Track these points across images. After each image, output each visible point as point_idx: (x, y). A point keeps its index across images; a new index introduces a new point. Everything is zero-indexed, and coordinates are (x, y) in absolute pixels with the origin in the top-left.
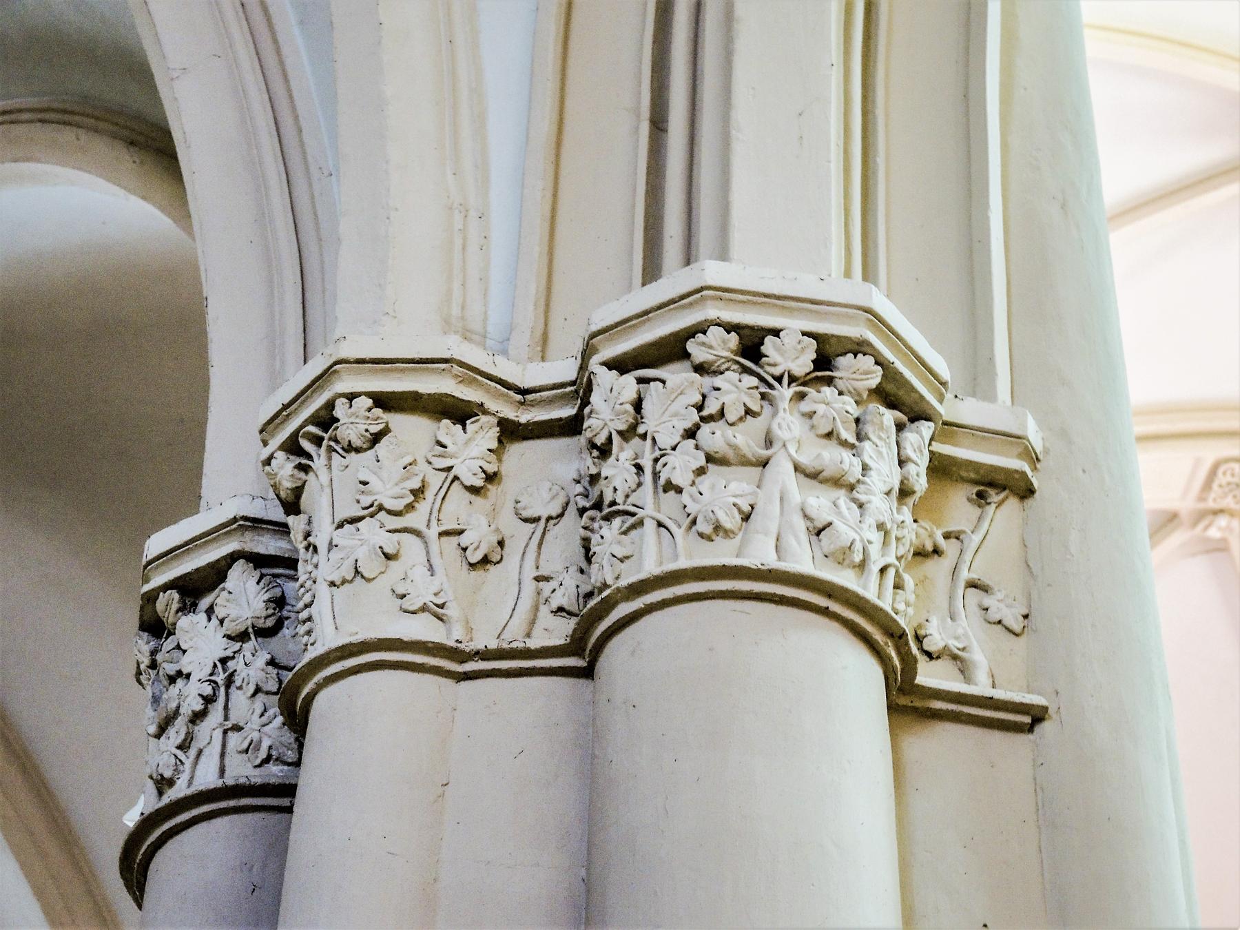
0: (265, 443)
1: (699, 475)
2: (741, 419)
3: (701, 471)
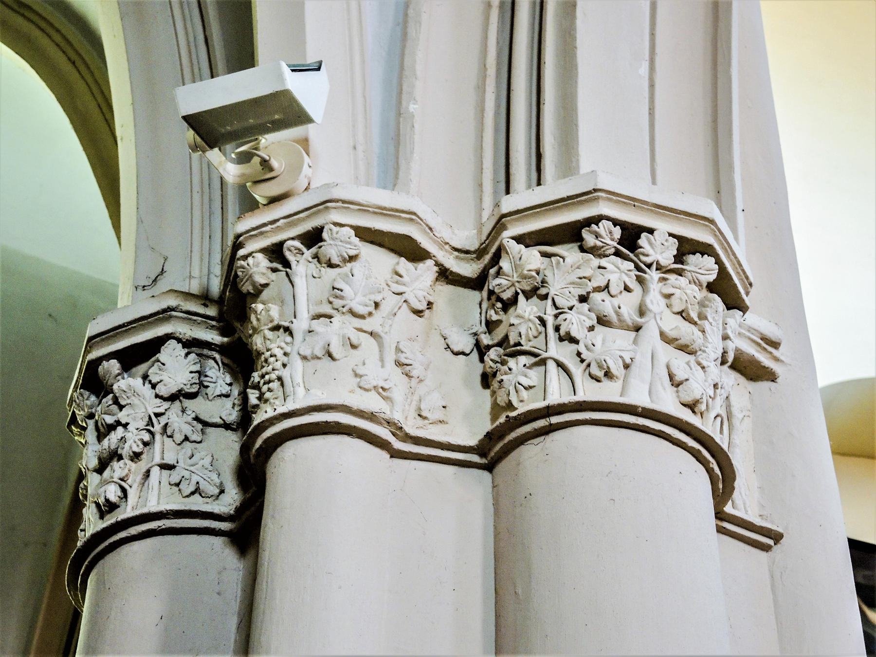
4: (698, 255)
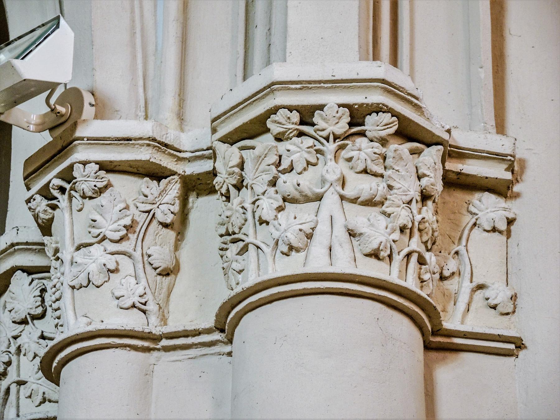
0: (28, 189)
1: (279, 211)
2: (305, 169)
3: (280, 209)
4: (374, 115)
